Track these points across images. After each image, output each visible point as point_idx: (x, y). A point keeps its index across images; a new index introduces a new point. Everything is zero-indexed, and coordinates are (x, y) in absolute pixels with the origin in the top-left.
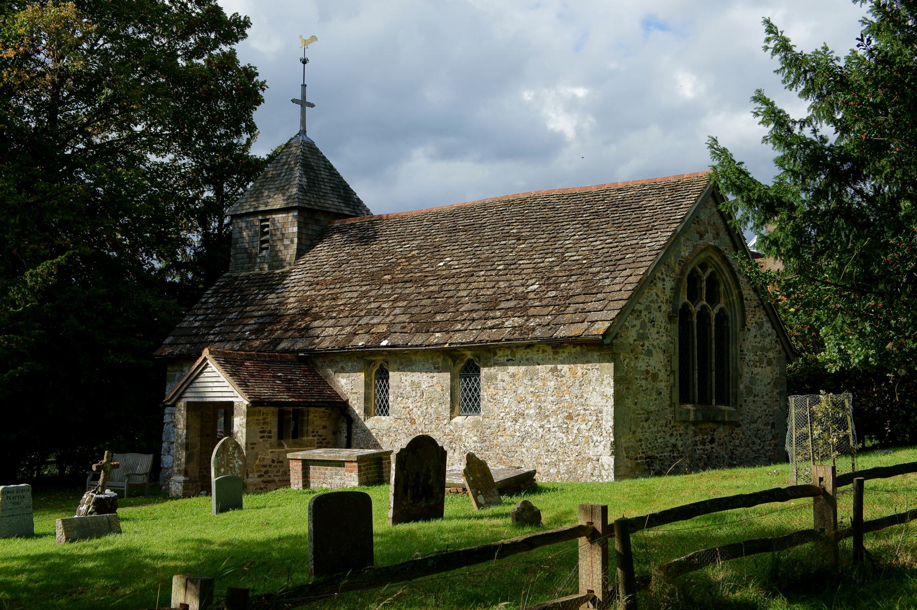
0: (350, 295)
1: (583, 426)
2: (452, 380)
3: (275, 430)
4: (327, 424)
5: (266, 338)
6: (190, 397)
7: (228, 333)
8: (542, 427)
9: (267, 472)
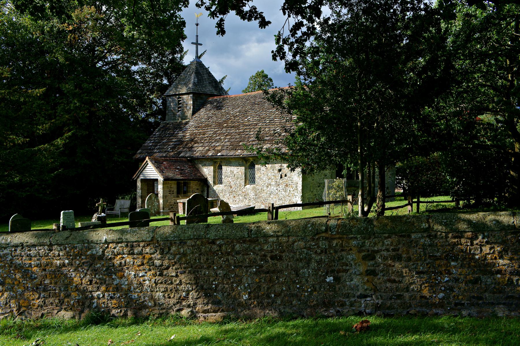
0: (210, 133)
1: (291, 189)
2: (214, 172)
3: (175, 190)
4: (199, 188)
5: (176, 151)
6: (142, 177)
7: (162, 149)
8: (277, 189)
9: (172, 208)
